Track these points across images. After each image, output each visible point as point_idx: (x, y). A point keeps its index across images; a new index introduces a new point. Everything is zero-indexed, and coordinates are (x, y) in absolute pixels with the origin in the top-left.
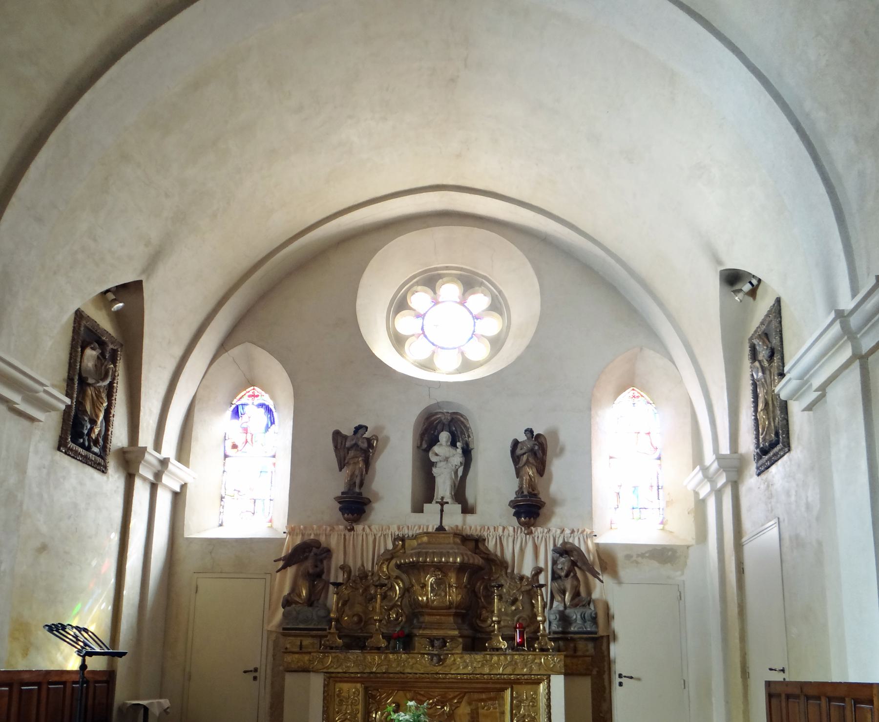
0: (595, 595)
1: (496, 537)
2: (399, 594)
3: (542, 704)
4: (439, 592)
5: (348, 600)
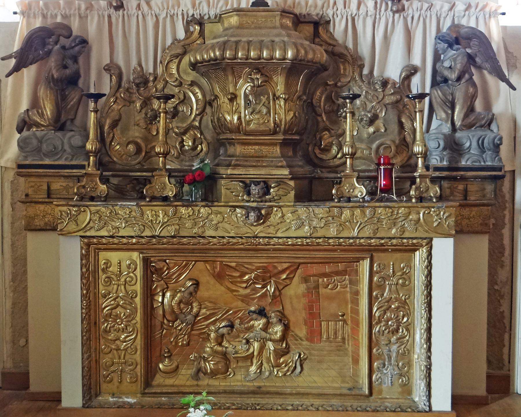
0: (497, 108)
1: (347, 16)
2: (197, 109)
3: (418, 282)
4: (258, 108)
5: (119, 120)
